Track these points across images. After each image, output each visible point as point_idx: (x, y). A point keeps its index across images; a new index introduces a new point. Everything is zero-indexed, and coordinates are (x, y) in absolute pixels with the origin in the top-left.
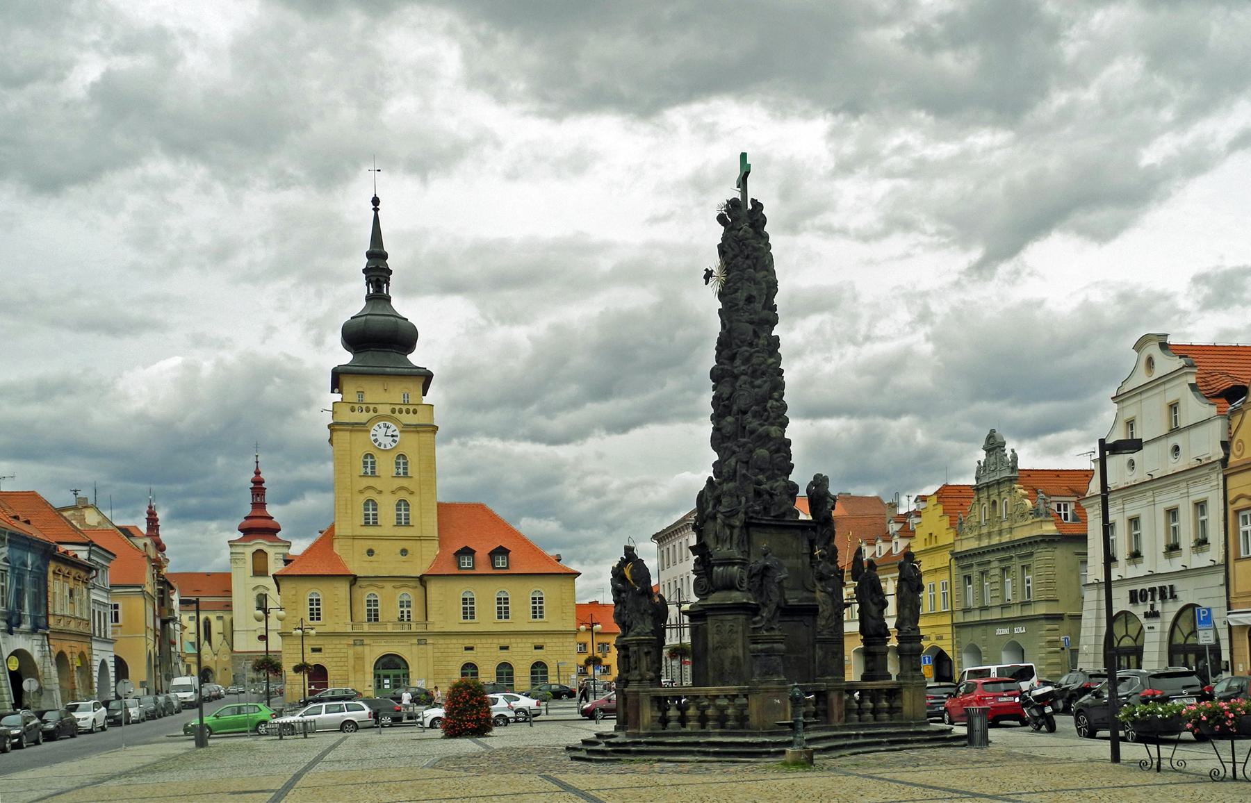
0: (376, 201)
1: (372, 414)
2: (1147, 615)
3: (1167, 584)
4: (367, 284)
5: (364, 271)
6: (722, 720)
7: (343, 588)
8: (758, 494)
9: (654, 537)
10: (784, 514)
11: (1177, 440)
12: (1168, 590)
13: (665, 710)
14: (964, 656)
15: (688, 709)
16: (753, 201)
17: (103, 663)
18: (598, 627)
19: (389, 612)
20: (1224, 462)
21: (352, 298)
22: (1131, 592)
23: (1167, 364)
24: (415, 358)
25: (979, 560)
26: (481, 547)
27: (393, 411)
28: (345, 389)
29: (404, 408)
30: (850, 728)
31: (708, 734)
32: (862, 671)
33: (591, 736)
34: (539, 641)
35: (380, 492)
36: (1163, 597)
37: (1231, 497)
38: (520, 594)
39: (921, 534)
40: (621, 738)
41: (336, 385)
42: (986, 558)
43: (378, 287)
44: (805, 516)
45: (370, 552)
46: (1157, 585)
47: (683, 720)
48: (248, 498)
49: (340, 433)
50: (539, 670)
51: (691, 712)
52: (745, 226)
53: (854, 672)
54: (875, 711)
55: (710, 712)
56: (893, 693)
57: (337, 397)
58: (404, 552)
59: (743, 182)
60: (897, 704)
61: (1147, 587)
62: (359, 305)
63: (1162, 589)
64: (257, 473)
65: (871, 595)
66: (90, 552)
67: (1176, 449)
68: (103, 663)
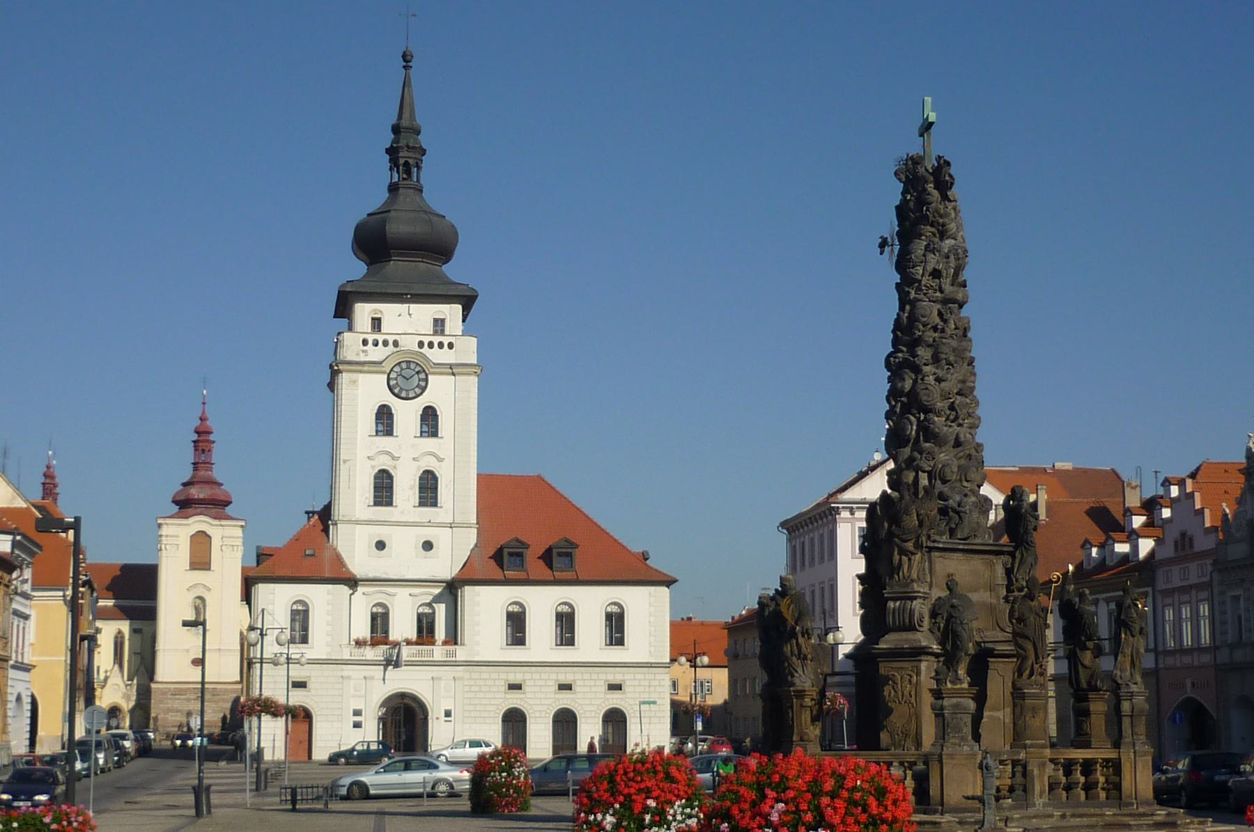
21: (368, 191)
24: (454, 270)
27: (421, 344)
29: (436, 340)
48: (383, 174)
62: (377, 198)
64: (48, 467)
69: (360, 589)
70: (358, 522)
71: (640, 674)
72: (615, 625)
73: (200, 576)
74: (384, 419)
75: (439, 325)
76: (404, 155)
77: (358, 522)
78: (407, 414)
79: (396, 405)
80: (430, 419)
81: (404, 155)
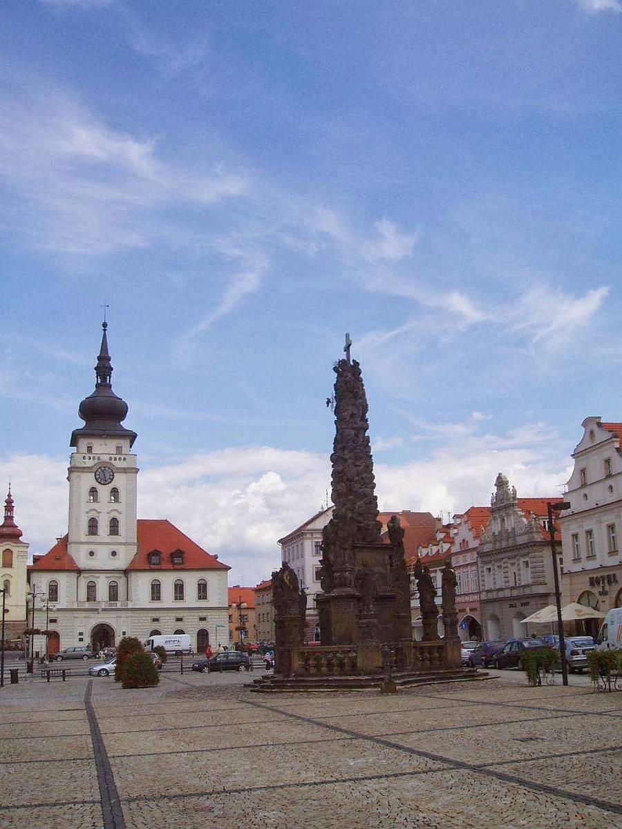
0: (105, 325)
1: (96, 461)
2: (601, 594)
3: (612, 573)
4: (97, 377)
5: (95, 369)
8: (359, 529)
9: (279, 541)
10: (375, 540)
11: (610, 482)
12: (612, 577)
14: (489, 622)
16: (354, 361)
18: (244, 605)
19: (102, 593)
22: (590, 578)
23: (602, 436)
24: (126, 424)
26: (165, 549)
27: (111, 459)
29: (118, 456)
30: (417, 670)
31: (333, 675)
32: (422, 635)
33: (259, 678)
34: (203, 614)
36: (610, 582)
38: (191, 581)
39: (458, 540)
40: (279, 677)
41: (74, 442)
43: (104, 379)
44: (388, 541)
45: (92, 554)
46: (606, 574)
48: (92, 379)
52: (349, 375)
53: (417, 636)
55: (334, 661)
56: (441, 648)
57: (74, 449)
58: (114, 554)
59: (347, 349)
61: (599, 575)
62: (91, 390)
63: (608, 576)
64: (9, 496)
65: (426, 586)
67: (611, 488)
69: (82, 575)
70: (81, 543)
72: (179, 590)
73: (7, 571)
74: (93, 491)
75: (119, 449)
76: (104, 369)
77: (81, 543)
78: (104, 491)
79: (99, 487)
80: (115, 491)
81: (104, 369)
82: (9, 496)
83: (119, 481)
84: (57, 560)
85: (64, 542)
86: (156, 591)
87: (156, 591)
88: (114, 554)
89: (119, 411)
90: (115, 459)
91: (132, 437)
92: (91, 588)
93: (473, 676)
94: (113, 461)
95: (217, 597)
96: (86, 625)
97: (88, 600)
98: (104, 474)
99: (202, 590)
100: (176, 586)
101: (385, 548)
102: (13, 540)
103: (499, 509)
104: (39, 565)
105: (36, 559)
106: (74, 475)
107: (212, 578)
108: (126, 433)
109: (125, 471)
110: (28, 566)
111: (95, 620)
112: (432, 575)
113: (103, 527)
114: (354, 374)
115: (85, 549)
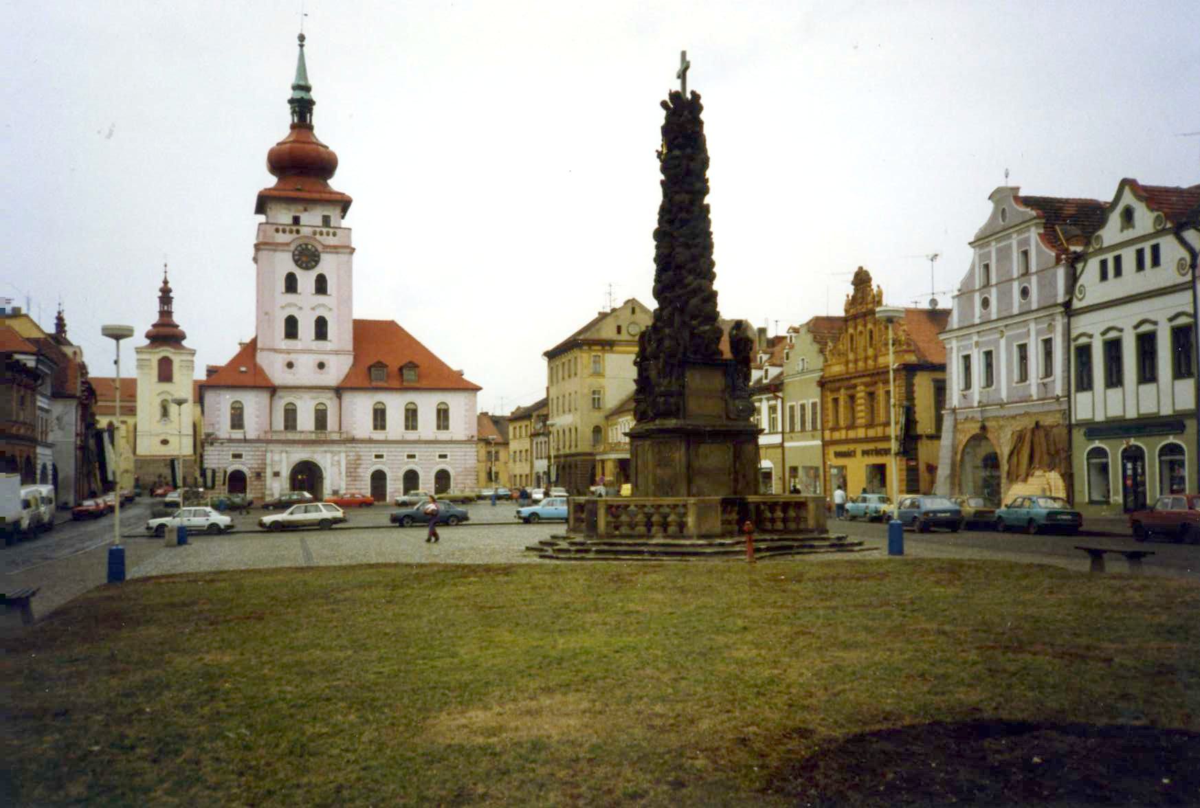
0: (302, 38)
6: (665, 526)
7: (264, 397)
13: (617, 517)
15: (636, 515)
16: (693, 93)
17: (44, 467)
19: (306, 421)
20: (1067, 305)
21: (279, 129)
24: (336, 183)
25: (846, 383)
26: (390, 360)
27: (315, 233)
28: (269, 212)
29: (325, 230)
35: (301, 308)
37: (1074, 334)
38: (427, 404)
42: (853, 382)
47: (632, 526)
48: (155, 306)
49: (265, 253)
50: (443, 479)
51: (671, 518)
54: (785, 520)
57: (262, 218)
58: (321, 366)
59: (682, 75)
60: (803, 514)
64: (166, 282)
66: (38, 361)
68: (44, 467)
70: (275, 350)
71: (423, 447)
72: (411, 417)
75: (326, 221)
76: (302, 107)
77: (275, 350)
78: (306, 280)
79: (299, 273)
81: (302, 107)
82: (166, 282)
83: (327, 265)
84: (243, 372)
85: (250, 350)
86: (380, 417)
87: (380, 417)
88: (290, 365)
89: (323, 165)
90: (321, 234)
91: (344, 204)
92: (291, 415)
93: (842, 545)
94: (318, 237)
95: (461, 426)
96: (284, 461)
97: (286, 428)
98: (307, 257)
99: (443, 416)
100: (407, 410)
101: (724, 366)
102: (752, 355)
103: (855, 317)
104: (216, 380)
105: (211, 371)
106: (263, 255)
107: (456, 403)
108: (333, 197)
109: (335, 249)
110: (195, 382)
111: (300, 454)
112: (757, 404)
113: (306, 328)
114: (691, 112)
115: (281, 360)
